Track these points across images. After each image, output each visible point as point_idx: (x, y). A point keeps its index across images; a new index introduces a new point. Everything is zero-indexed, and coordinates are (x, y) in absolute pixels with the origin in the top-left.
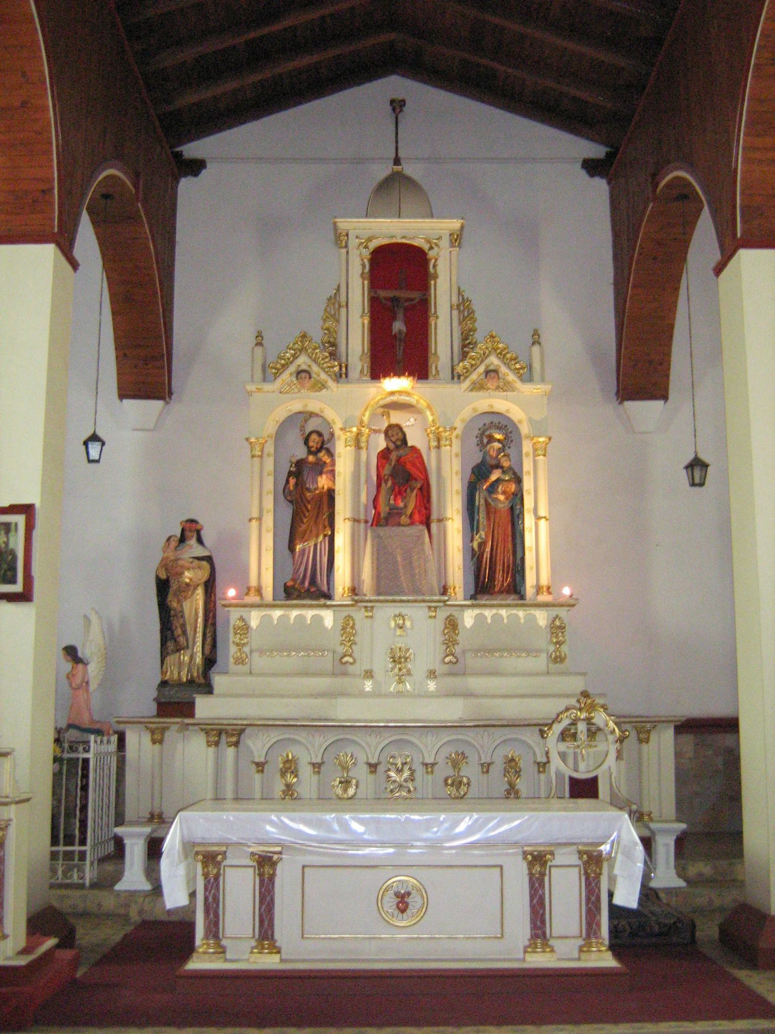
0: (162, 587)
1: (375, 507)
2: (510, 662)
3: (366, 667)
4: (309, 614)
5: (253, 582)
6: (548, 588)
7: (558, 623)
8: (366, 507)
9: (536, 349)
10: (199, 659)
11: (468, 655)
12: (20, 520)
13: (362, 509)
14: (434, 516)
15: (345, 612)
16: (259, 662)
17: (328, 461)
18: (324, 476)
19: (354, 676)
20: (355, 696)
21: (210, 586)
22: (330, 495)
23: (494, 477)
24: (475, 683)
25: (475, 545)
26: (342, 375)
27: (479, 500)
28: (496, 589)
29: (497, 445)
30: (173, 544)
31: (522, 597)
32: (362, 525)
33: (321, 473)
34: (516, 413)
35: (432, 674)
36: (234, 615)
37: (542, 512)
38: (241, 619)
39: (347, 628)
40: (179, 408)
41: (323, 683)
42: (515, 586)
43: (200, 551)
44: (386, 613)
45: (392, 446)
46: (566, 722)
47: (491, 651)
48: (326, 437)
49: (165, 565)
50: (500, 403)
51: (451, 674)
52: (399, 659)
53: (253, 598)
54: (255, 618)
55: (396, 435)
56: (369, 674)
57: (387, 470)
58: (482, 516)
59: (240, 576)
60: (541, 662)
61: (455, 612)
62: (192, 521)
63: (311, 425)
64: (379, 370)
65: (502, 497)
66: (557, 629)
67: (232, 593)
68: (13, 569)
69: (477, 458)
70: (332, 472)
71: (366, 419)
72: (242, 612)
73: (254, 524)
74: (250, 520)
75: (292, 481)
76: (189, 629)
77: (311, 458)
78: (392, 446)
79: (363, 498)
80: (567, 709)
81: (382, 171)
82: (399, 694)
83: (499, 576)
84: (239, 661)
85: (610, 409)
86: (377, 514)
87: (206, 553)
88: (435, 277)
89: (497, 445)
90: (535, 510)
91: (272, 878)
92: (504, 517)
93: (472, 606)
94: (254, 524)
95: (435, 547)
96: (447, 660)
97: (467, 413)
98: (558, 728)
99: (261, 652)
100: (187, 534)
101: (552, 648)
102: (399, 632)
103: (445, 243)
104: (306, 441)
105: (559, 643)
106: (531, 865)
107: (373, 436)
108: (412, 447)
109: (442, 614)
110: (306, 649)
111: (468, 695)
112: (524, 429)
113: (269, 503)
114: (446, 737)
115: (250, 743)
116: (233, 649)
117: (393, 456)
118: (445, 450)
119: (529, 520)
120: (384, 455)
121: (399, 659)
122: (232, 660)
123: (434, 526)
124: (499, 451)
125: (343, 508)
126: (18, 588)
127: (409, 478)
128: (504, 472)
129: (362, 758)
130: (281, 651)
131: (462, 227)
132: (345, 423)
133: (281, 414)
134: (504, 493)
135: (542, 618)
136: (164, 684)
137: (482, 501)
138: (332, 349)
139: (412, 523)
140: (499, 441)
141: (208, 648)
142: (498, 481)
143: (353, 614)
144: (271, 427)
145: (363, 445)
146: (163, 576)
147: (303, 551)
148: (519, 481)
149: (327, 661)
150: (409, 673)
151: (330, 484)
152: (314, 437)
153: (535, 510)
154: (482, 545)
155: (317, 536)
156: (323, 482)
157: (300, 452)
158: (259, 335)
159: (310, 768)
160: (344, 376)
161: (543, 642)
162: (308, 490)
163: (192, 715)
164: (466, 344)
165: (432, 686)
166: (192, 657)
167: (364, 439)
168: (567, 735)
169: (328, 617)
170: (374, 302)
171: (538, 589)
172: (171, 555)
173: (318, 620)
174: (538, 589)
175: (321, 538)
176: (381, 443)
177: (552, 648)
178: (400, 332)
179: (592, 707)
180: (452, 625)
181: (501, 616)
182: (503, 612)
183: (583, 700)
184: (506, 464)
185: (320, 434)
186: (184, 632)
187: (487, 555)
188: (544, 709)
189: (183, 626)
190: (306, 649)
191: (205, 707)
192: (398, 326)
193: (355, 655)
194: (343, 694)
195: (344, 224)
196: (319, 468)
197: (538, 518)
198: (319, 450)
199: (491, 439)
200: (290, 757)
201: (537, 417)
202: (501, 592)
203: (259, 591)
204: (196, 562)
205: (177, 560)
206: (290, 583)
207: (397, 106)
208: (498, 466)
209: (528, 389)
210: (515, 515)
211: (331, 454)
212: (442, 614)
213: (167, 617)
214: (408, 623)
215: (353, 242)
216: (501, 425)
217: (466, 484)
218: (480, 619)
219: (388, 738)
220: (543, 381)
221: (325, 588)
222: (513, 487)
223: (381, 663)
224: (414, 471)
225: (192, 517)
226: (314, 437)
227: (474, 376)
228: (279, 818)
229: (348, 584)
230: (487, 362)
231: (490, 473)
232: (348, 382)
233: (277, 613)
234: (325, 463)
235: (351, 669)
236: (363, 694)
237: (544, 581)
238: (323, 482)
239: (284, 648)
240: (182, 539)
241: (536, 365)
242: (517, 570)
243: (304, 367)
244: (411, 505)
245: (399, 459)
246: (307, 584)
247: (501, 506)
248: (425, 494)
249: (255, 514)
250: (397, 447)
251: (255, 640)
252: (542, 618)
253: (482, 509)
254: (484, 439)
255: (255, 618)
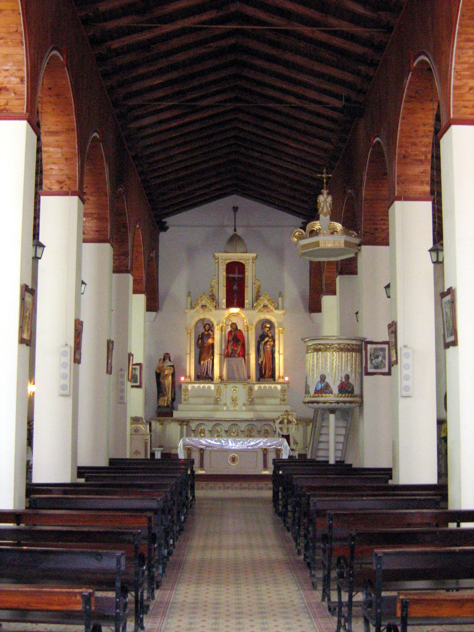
0: (158, 375)
1: (227, 349)
2: (269, 401)
3: (225, 402)
4: (206, 386)
5: (188, 374)
6: (283, 377)
7: (284, 389)
8: (224, 350)
9: (280, 299)
10: (170, 399)
11: (256, 399)
12: (138, 367)
13: (223, 351)
14: (246, 353)
15: (217, 386)
16: (192, 400)
17: (212, 333)
18: (211, 339)
19: (220, 405)
20: (221, 411)
21: (173, 375)
22: (212, 345)
23: (266, 339)
24: (257, 407)
25: (260, 362)
26: (217, 307)
27: (261, 347)
28: (266, 376)
29: (267, 329)
30: (162, 361)
31: (274, 380)
32: (223, 356)
33: (209, 338)
34: (273, 320)
35: (244, 405)
36: (183, 386)
37: (281, 352)
38: (185, 387)
39: (218, 391)
40: (161, 314)
41: (211, 407)
42: (273, 375)
43: (170, 364)
44: (230, 386)
45: (233, 330)
46: (281, 419)
47: (262, 397)
48: (211, 325)
49: (159, 368)
50: (268, 316)
51: (250, 404)
52: (234, 400)
53: (188, 380)
54: (190, 387)
55: (234, 326)
56: (225, 404)
57: (231, 338)
58: (262, 352)
59: (184, 374)
60: (278, 401)
61: (252, 386)
62: (167, 354)
63: (205, 322)
64: (229, 305)
65: (268, 346)
66: (283, 391)
67: (183, 379)
68: (137, 379)
69: (260, 333)
70: (213, 338)
71: (224, 321)
72: (186, 385)
73: (188, 355)
74: (187, 354)
75: (200, 341)
76: (167, 388)
77: (206, 333)
78: (233, 330)
79: (223, 347)
80: (281, 415)
81: (231, 232)
82: (234, 411)
83: (267, 372)
84: (185, 400)
85: (306, 315)
86: (228, 352)
87: (172, 364)
88: (247, 287)
89: (267, 329)
90: (279, 351)
91: (203, 453)
92: (270, 352)
93: (257, 384)
94: (188, 355)
95: (247, 365)
96: (249, 400)
97: (257, 319)
98: (279, 421)
99: (192, 397)
100: (166, 358)
101: (282, 397)
102: (234, 392)
103: (251, 261)
104: (204, 327)
105: (284, 395)
106: (263, 451)
107: (227, 327)
108: (239, 330)
109: (248, 386)
110: (206, 397)
111: (256, 411)
112: (276, 325)
113: (193, 349)
114: (247, 423)
115: (190, 424)
116: (183, 396)
117: (233, 333)
118: (250, 332)
119: (277, 355)
120: (230, 332)
121: (234, 400)
122: (183, 400)
123: (246, 357)
124: (268, 331)
125: (217, 351)
126: (138, 384)
127: (238, 341)
128: (269, 338)
129: (223, 429)
130: (198, 397)
131: (257, 256)
132: (217, 323)
133: (196, 319)
134: (269, 345)
135: (279, 387)
136: (159, 407)
137: (262, 348)
138: (213, 297)
139: (239, 356)
140: (268, 327)
141: (173, 395)
142: (268, 341)
143: (220, 386)
144: (193, 324)
145: (224, 330)
146: (158, 372)
147: (203, 364)
148: (274, 341)
149: (212, 400)
150: (237, 404)
151: (213, 342)
152: (207, 326)
153: (279, 351)
154: (262, 362)
155: (208, 359)
156: (210, 341)
157: (202, 330)
158: (189, 293)
159: (208, 432)
160: (260, 610)
161: (279, 395)
162: (205, 343)
163: (172, 416)
164: (257, 297)
165: (244, 408)
166: (168, 398)
167: (224, 328)
168: (281, 422)
169: (212, 387)
170: (228, 278)
171: (279, 377)
172: (161, 365)
173: (209, 387)
174: (279, 377)
175: (209, 359)
176: (229, 329)
177: (282, 397)
178: (236, 289)
179: (289, 415)
180: (251, 389)
181: (266, 387)
182: (267, 385)
183: (286, 413)
184: (270, 335)
185: (209, 325)
186: (165, 390)
187: (263, 366)
188: (275, 415)
189: (165, 388)
190: (206, 397)
191: (176, 414)
192: (235, 287)
193: (221, 399)
194: (217, 410)
195: (217, 255)
196: (209, 336)
197: (280, 354)
198: (209, 330)
199: (266, 327)
200: (158, 456)
201: (280, 321)
202: (268, 377)
203: (190, 377)
204: (169, 367)
205: (163, 367)
206: (199, 374)
207: (235, 209)
208: (268, 336)
209: (277, 312)
210: (273, 352)
211: (213, 331)
212: (248, 386)
213: (159, 385)
214: (237, 389)
215: (220, 261)
216: (164, 576)
217: (257, 342)
218: (260, 387)
219: (230, 423)
220: (283, 309)
221: (211, 376)
222: (272, 343)
223: (229, 401)
224: (241, 339)
225: (167, 352)
226: (207, 326)
227: (260, 308)
228: (206, 441)
229: (218, 375)
230: (264, 303)
231: (265, 338)
232: (218, 309)
233: (196, 385)
234: (210, 334)
235: (220, 402)
236: (223, 411)
237: (281, 374)
238: (210, 341)
239: (199, 397)
240: (164, 359)
241: (280, 304)
242: (273, 370)
243: (204, 304)
244: (239, 351)
245: (235, 334)
246: (205, 374)
247: (268, 349)
248: (243, 345)
249: (188, 352)
250: (235, 330)
251: (190, 394)
252: (279, 387)
253: (262, 350)
254: (263, 327)
255: (190, 387)
